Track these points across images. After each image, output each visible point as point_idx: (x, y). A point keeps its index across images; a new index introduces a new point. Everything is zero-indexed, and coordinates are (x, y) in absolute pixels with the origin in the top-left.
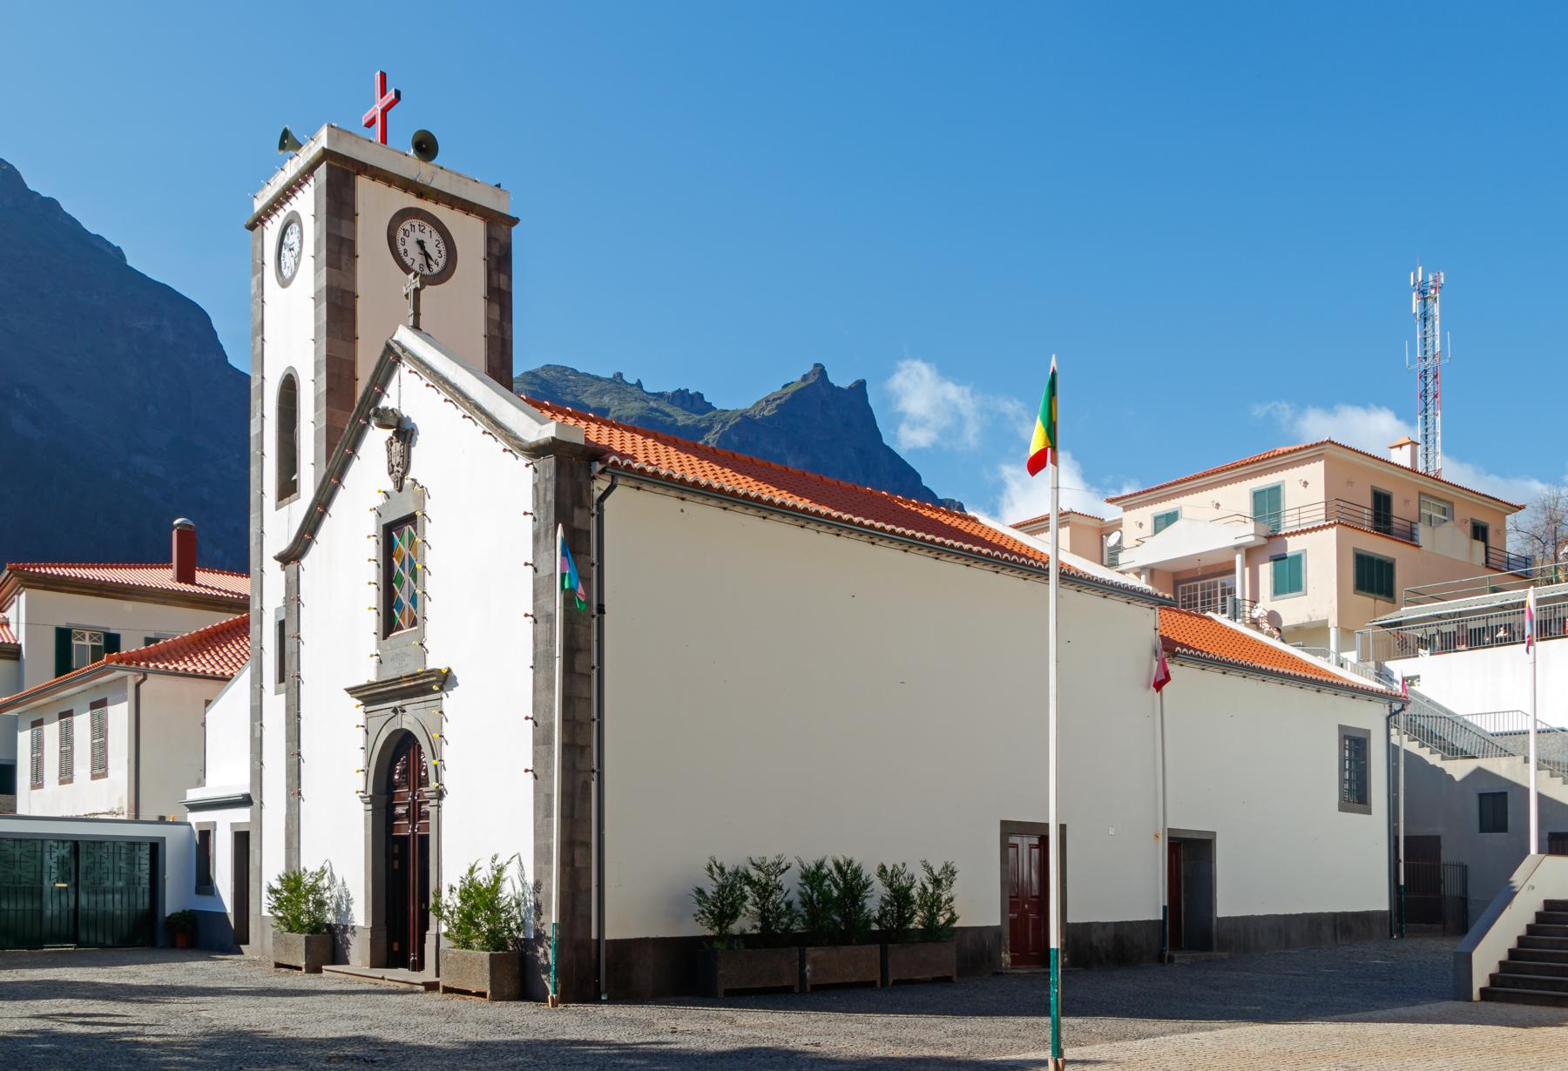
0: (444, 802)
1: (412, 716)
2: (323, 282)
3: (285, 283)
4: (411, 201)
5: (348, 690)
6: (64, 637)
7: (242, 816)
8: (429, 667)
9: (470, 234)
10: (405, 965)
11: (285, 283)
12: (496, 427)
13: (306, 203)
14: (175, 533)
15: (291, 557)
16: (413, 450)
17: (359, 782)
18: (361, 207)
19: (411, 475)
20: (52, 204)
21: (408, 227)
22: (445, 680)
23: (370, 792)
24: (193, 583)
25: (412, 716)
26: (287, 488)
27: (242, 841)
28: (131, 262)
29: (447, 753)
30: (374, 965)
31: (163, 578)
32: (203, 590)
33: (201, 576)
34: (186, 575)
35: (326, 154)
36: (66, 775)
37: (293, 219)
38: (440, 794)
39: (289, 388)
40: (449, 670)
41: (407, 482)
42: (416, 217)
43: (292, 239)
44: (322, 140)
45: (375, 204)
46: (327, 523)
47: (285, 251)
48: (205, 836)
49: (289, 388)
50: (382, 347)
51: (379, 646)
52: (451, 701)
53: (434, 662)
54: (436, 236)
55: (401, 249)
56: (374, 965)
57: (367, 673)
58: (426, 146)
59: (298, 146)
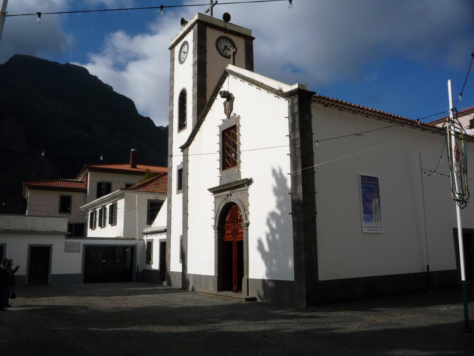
0: (249, 227)
1: (235, 197)
2: (196, 59)
3: (181, 62)
4: (222, 34)
5: (208, 190)
6: (99, 185)
7: (163, 236)
9: (240, 43)
10: (230, 289)
11: (181, 62)
12: (270, 89)
13: (190, 38)
14: (131, 154)
15: (185, 148)
16: (234, 103)
17: (212, 222)
18: (208, 36)
19: (234, 112)
20: (96, 77)
21: (221, 42)
22: (249, 182)
23: (217, 226)
24: (136, 168)
26: (182, 126)
27: (164, 246)
28: (115, 90)
29: (251, 209)
30: (219, 290)
31: (127, 167)
32: (139, 170)
33: (138, 166)
34: (134, 166)
35: (198, 21)
37: (186, 43)
38: (248, 225)
39: (183, 95)
40: (251, 179)
41: (232, 115)
42: (224, 39)
43: (185, 49)
44: (196, 17)
45: (212, 36)
47: (182, 54)
48: (150, 244)
49: (183, 95)
50: (223, 71)
51: (220, 173)
52: (251, 189)
53: (244, 176)
54: (230, 44)
55: (220, 48)
56: (219, 290)
57: (216, 183)
59: (187, 22)
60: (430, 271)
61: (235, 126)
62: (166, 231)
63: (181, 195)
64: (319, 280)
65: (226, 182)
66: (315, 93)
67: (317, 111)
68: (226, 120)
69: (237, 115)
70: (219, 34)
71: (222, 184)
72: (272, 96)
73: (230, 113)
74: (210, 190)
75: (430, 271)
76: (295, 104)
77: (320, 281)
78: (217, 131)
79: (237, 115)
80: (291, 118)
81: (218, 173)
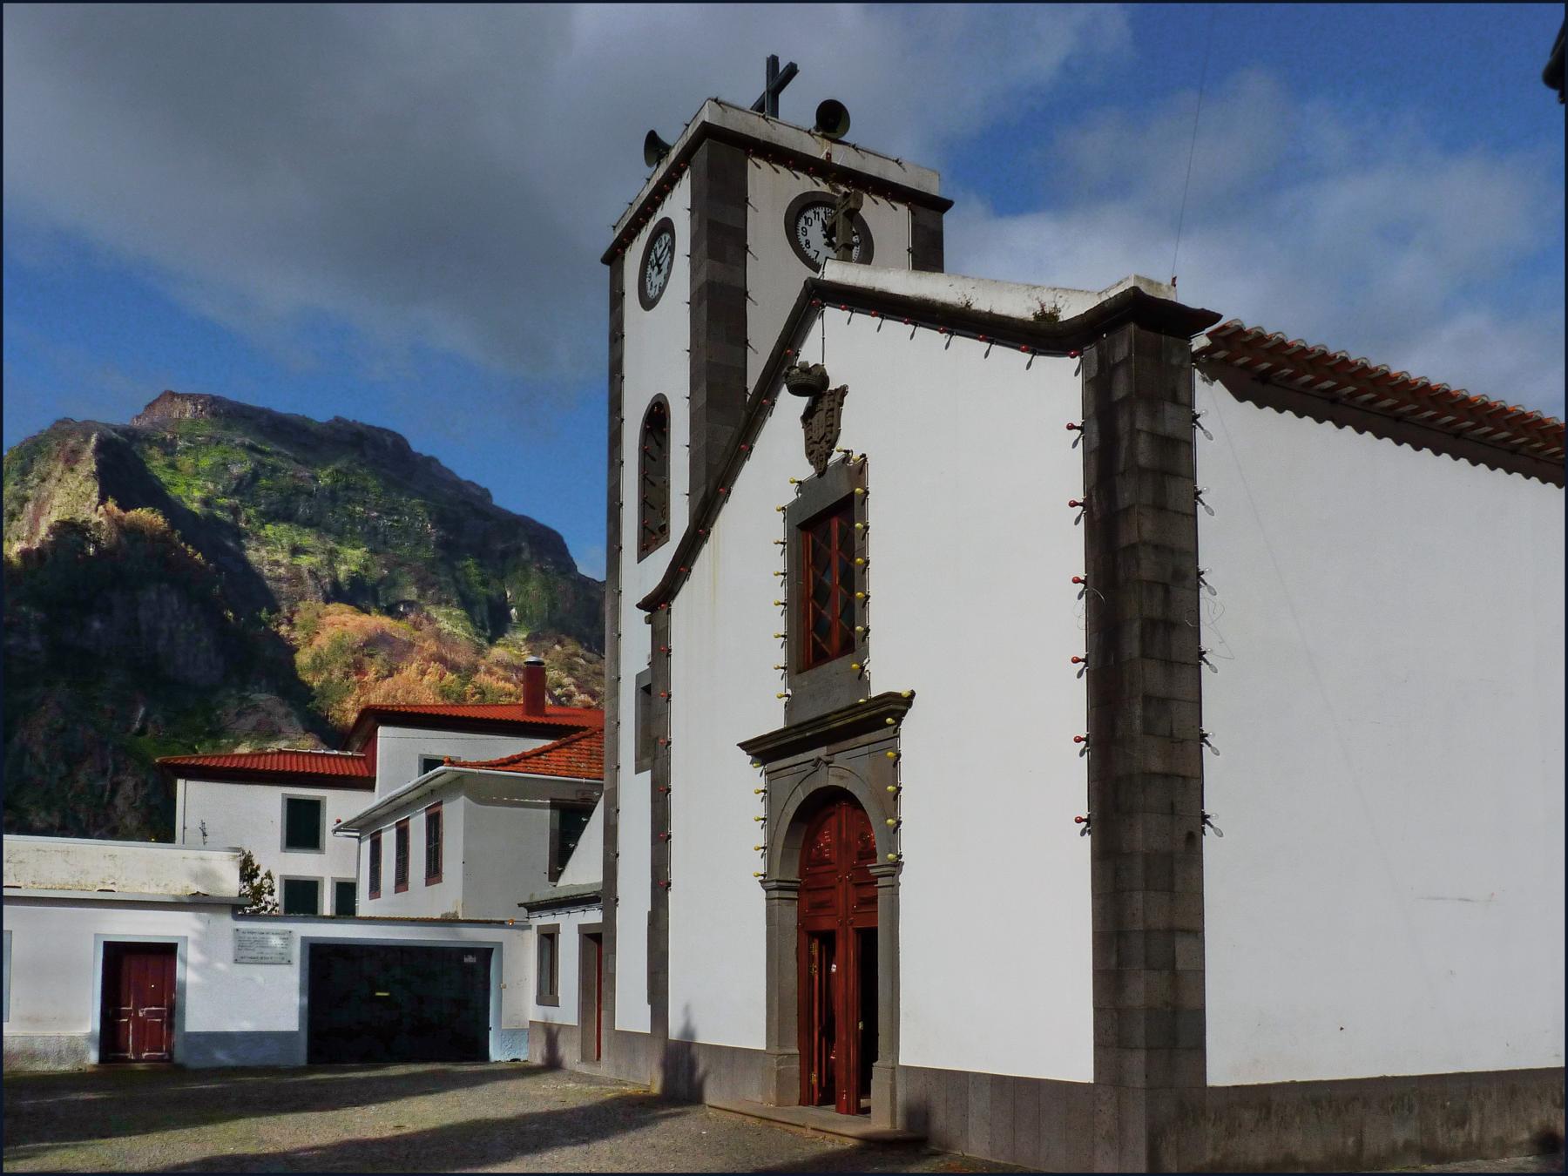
3: (648, 303)
7: (594, 916)
8: (875, 691)
11: (648, 303)
13: (678, 206)
15: (658, 604)
22: (898, 705)
25: (844, 768)
26: (652, 535)
36: (402, 882)
37: (666, 226)
38: (897, 865)
39: (657, 417)
41: (836, 456)
45: (771, 192)
46: (706, 551)
49: (657, 417)
53: (878, 687)
55: (803, 240)
57: (771, 719)
58: (832, 118)
60: (1245, 1042)
61: (851, 497)
62: (605, 896)
63: (647, 776)
64: (1210, 1083)
65: (809, 713)
66: (1219, 317)
67: (1232, 437)
68: (810, 481)
69: (856, 456)
70: (806, 184)
71: (796, 722)
72: (1009, 359)
73: (829, 455)
74: (741, 745)
75: (1245, 1042)
76: (1117, 366)
77: (1213, 1088)
78: (777, 529)
79: (856, 456)
80: (1094, 428)
81: (777, 685)
